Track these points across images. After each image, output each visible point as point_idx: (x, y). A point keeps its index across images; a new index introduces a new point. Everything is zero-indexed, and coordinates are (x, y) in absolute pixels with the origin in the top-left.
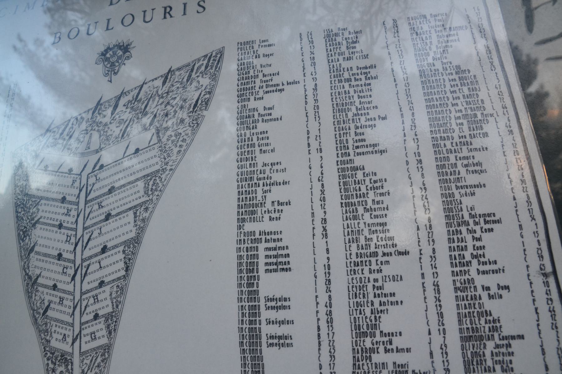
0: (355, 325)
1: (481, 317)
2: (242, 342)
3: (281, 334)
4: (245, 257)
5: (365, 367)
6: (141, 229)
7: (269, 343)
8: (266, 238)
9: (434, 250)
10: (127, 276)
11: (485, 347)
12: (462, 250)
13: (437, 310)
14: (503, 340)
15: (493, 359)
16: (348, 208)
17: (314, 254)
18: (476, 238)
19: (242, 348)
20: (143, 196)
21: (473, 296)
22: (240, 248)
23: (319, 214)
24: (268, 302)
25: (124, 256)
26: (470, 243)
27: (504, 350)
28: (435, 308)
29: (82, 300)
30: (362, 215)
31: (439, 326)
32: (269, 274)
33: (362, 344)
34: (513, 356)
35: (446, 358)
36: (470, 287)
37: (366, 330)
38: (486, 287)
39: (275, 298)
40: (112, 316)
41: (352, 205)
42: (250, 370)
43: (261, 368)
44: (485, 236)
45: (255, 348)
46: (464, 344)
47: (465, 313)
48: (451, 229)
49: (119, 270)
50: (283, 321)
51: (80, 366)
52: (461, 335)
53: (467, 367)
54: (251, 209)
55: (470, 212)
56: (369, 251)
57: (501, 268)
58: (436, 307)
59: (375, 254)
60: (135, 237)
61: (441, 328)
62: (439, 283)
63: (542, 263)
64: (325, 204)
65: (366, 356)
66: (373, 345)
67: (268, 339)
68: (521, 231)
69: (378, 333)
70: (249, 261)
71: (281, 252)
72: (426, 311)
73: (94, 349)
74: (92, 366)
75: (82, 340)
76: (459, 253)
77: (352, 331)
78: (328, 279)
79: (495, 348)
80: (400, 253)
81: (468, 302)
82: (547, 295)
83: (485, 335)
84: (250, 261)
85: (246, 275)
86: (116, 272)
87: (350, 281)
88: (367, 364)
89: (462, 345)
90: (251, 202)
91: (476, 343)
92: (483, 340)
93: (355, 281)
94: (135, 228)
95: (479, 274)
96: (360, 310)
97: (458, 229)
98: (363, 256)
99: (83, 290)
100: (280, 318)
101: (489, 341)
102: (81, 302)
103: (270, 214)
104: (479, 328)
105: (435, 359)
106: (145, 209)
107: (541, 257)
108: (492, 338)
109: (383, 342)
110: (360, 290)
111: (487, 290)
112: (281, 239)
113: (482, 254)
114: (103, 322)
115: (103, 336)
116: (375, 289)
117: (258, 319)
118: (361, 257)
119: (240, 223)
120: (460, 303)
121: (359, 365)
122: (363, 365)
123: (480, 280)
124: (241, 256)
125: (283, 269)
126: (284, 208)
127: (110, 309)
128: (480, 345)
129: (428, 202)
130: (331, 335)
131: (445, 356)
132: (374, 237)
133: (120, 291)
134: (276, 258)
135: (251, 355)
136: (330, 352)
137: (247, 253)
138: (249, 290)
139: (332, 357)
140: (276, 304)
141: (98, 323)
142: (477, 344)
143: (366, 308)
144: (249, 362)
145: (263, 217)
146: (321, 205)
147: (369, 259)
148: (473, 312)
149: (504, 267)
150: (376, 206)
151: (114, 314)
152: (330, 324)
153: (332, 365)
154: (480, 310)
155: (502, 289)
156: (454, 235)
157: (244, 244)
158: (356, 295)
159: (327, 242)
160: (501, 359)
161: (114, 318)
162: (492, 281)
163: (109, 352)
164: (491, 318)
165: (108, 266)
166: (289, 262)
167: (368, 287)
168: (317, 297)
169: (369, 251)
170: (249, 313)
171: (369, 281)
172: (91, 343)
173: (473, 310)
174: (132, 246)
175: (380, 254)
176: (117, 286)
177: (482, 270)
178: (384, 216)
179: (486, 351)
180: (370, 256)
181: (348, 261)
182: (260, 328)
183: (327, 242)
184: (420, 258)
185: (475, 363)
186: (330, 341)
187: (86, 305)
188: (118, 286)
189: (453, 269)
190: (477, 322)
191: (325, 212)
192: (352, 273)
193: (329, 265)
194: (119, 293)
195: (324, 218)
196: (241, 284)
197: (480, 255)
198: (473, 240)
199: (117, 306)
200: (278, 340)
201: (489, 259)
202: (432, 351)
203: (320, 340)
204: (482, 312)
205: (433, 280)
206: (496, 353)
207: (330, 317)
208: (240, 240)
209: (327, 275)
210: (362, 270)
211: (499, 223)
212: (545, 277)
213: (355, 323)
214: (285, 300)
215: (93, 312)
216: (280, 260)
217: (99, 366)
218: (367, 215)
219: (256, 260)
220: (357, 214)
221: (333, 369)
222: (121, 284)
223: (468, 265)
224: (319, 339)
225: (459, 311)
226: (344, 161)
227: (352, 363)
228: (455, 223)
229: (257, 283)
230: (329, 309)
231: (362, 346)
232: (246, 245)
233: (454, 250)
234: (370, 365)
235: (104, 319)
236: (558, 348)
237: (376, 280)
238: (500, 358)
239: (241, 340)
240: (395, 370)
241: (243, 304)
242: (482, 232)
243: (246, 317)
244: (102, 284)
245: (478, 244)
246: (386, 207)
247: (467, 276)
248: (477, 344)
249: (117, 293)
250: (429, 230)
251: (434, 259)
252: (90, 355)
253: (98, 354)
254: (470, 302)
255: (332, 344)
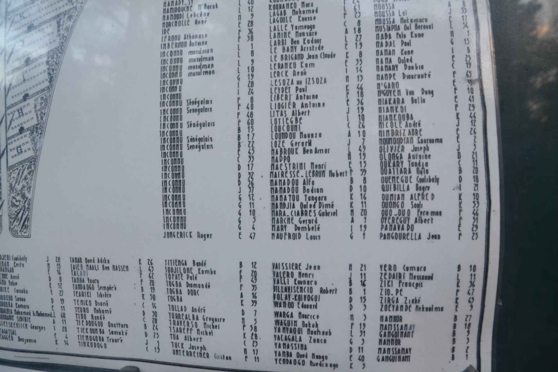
0: (276, 126)
1: (402, 120)
2: (164, 146)
3: (201, 136)
4: (169, 62)
5: (283, 168)
6: (65, 39)
7: (189, 146)
8: (191, 41)
9: (361, 53)
10: (51, 87)
11: (403, 150)
12: (390, 54)
13: (359, 112)
14: (422, 143)
15: (409, 161)
16: (276, 11)
17: (239, 57)
18: (405, 43)
19: (163, 151)
20: (67, 4)
21: (396, 99)
22: (164, 53)
23: (246, 16)
24: (190, 104)
25: (47, 66)
26: (398, 48)
27: (421, 153)
28: (357, 110)
29: (7, 115)
30: (290, 18)
31: (359, 127)
32: (192, 78)
33: (281, 145)
34: (429, 158)
35: (364, 159)
36: (394, 91)
37: (286, 131)
38: (410, 92)
39: (197, 100)
40: (37, 128)
41: (280, 8)
42: (171, 172)
43: (181, 170)
44: (414, 41)
45: (176, 151)
46: (383, 146)
47: (387, 116)
48: (380, 33)
49: (43, 82)
50: (204, 123)
51: (8, 180)
52: (381, 137)
53: (384, 168)
54: (177, 13)
55: (402, 16)
56: (294, 53)
57: (428, 73)
58: (357, 110)
59: (301, 57)
60: (59, 47)
61: (361, 130)
62: (362, 87)
63: (469, 70)
64: (252, 7)
65: (285, 157)
66: (292, 145)
67: (188, 142)
68: (452, 37)
69: (298, 134)
70: (173, 65)
71: (205, 55)
72: (348, 113)
73: (21, 162)
74: (19, 180)
75: (9, 154)
76: (386, 57)
77: (272, 132)
78: (251, 81)
79: (412, 151)
80: (326, 56)
81: (390, 105)
82: (470, 101)
83: (405, 138)
84: (174, 65)
85: (169, 79)
86: (40, 84)
87: (273, 83)
88: (286, 164)
89: (381, 147)
90: (177, 7)
91: (394, 145)
92: (401, 143)
93: (278, 83)
94: (59, 38)
95: (404, 78)
96: (282, 111)
97: (388, 33)
98: (288, 58)
99: (8, 105)
100: (201, 121)
101: (408, 144)
102: (6, 117)
103: (196, 18)
104: (399, 131)
105: (352, 160)
106: (68, 17)
107: (469, 64)
108: (411, 141)
109: (303, 143)
110: (282, 92)
111: (410, 94)
112: (206, 42)
113: (409, 59)
114: (28, 136)
115: (29, 149)
116: (298, 91)
117: (179, 122)
118: (286, 59)
119: (165, 28)
120: (382, 106)
121: (277, 165)
122: (281, 165)
123: (404, 85)
124: (164, 60)
125: (206, 72)
126: (211, 11)
127: (35, 122)
128: (399, 147)
129: (359, 6)
130: (251, 136)
131: (363, 157)
132: (301, 39)
133: (44, 103)
134: (200, 61)
135: (172, 158)
136: (249, 153)
137: (171, 57)
138: (171, 94)
139: (251, 157)
140: (198, 106)
141: (23, 137)
142: (395, 147)
143: (287, 109)
144: (169, 165)
145: (188, 21)
146: (249, 8)
147: (294, 61)
148: (395, 116)
149: (430, 72)
150: (306, 9)
151: (39, 126)
152: (250, 126)
153: (251, 166)
154: (401, 114)
155: (426, 94)
156: (383, 38)
157: (168, 48)
158: (278, 97)
159: (252, 44)
160: (418, 162)
161: (39, 130)
162: (416, 86)
163: (35, 164)
164: (412, 122)
165: (31, 78)
166: (212, 65)
167: (291, 89)
168: (239, 99)
169: (294, 53)
170: (171, 116)
171: (292, 83)
172: (18, 157)
173: (395, 113)
174: (55, 56)
175: (306, 56)
176: (41, 98)
177: (408, 75)
178: (313, 18)
179: (403, 154)
180: (296, 59)
181: (273, 64)
182: (181, 131)
183: (252, 44)
184: (346, 61)
185: (391, 165)
186: (250, 142)
187: (12, 120)
188: (42, 98)
189: (378, 73)
190: (398, 125)
191: (252, 15)
192: (276, 75)
193: (253, 67)
194: (43, 105)
195: (250, 20)
196: (164, 88)
197: (408, 60)
198: (402, 44)
199: (42, 118)
200: (198, 142)
201: (416, 64)
202: (350, 152)
203: (240, 141)
204: (404, 116)
205: (357, 83)
206: (413, 156)
207: (250, 119)
208: (165, 45)
209: (251, 77)
210: (286, 72)
211: (430, 28)
212: (470, 84)
213: (276, 124)
214: (207, 102)
215: (18, 125)
216: (204, 63)
217: (26, 179)
218: (295, 17)
219: (179, 64)
220: (285, 16)
221: (252, 169)
222: (45, 95)
223: (394, 69)
224: (239, 140)
225: (380, 114)
226: (277, 5)
227: (271, 163)
228: (386, 27)
229: (180, 87)
230: (250, 110)
231: (282, 147)
232: (170, 49)
233: (382, 54)
234: (288, 166)
235: (29, 132)
236: (473, 153)
237: (299, 83)
238: (417, 161)
239: (163, 144)
240: (312, 170)
241: (166, 108)
242: (412, 37)
243: (168, 121)
244: (26, 97)
245: (407, 48)
246: (315, 9)
247: (392, 80)
248: (395, 147)
249: (41, 105)
250: (357, 33)
251: (360, 62)
252: (17, 169)
253: (24, 167)
254: (392, 105)
255: (251, 145)
